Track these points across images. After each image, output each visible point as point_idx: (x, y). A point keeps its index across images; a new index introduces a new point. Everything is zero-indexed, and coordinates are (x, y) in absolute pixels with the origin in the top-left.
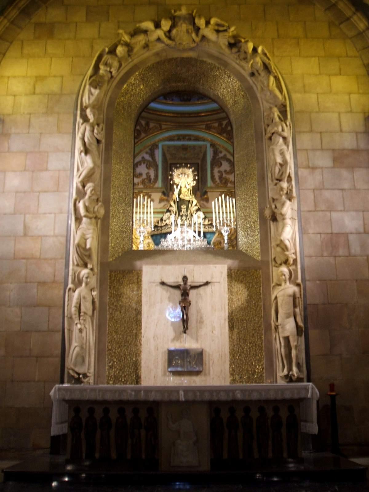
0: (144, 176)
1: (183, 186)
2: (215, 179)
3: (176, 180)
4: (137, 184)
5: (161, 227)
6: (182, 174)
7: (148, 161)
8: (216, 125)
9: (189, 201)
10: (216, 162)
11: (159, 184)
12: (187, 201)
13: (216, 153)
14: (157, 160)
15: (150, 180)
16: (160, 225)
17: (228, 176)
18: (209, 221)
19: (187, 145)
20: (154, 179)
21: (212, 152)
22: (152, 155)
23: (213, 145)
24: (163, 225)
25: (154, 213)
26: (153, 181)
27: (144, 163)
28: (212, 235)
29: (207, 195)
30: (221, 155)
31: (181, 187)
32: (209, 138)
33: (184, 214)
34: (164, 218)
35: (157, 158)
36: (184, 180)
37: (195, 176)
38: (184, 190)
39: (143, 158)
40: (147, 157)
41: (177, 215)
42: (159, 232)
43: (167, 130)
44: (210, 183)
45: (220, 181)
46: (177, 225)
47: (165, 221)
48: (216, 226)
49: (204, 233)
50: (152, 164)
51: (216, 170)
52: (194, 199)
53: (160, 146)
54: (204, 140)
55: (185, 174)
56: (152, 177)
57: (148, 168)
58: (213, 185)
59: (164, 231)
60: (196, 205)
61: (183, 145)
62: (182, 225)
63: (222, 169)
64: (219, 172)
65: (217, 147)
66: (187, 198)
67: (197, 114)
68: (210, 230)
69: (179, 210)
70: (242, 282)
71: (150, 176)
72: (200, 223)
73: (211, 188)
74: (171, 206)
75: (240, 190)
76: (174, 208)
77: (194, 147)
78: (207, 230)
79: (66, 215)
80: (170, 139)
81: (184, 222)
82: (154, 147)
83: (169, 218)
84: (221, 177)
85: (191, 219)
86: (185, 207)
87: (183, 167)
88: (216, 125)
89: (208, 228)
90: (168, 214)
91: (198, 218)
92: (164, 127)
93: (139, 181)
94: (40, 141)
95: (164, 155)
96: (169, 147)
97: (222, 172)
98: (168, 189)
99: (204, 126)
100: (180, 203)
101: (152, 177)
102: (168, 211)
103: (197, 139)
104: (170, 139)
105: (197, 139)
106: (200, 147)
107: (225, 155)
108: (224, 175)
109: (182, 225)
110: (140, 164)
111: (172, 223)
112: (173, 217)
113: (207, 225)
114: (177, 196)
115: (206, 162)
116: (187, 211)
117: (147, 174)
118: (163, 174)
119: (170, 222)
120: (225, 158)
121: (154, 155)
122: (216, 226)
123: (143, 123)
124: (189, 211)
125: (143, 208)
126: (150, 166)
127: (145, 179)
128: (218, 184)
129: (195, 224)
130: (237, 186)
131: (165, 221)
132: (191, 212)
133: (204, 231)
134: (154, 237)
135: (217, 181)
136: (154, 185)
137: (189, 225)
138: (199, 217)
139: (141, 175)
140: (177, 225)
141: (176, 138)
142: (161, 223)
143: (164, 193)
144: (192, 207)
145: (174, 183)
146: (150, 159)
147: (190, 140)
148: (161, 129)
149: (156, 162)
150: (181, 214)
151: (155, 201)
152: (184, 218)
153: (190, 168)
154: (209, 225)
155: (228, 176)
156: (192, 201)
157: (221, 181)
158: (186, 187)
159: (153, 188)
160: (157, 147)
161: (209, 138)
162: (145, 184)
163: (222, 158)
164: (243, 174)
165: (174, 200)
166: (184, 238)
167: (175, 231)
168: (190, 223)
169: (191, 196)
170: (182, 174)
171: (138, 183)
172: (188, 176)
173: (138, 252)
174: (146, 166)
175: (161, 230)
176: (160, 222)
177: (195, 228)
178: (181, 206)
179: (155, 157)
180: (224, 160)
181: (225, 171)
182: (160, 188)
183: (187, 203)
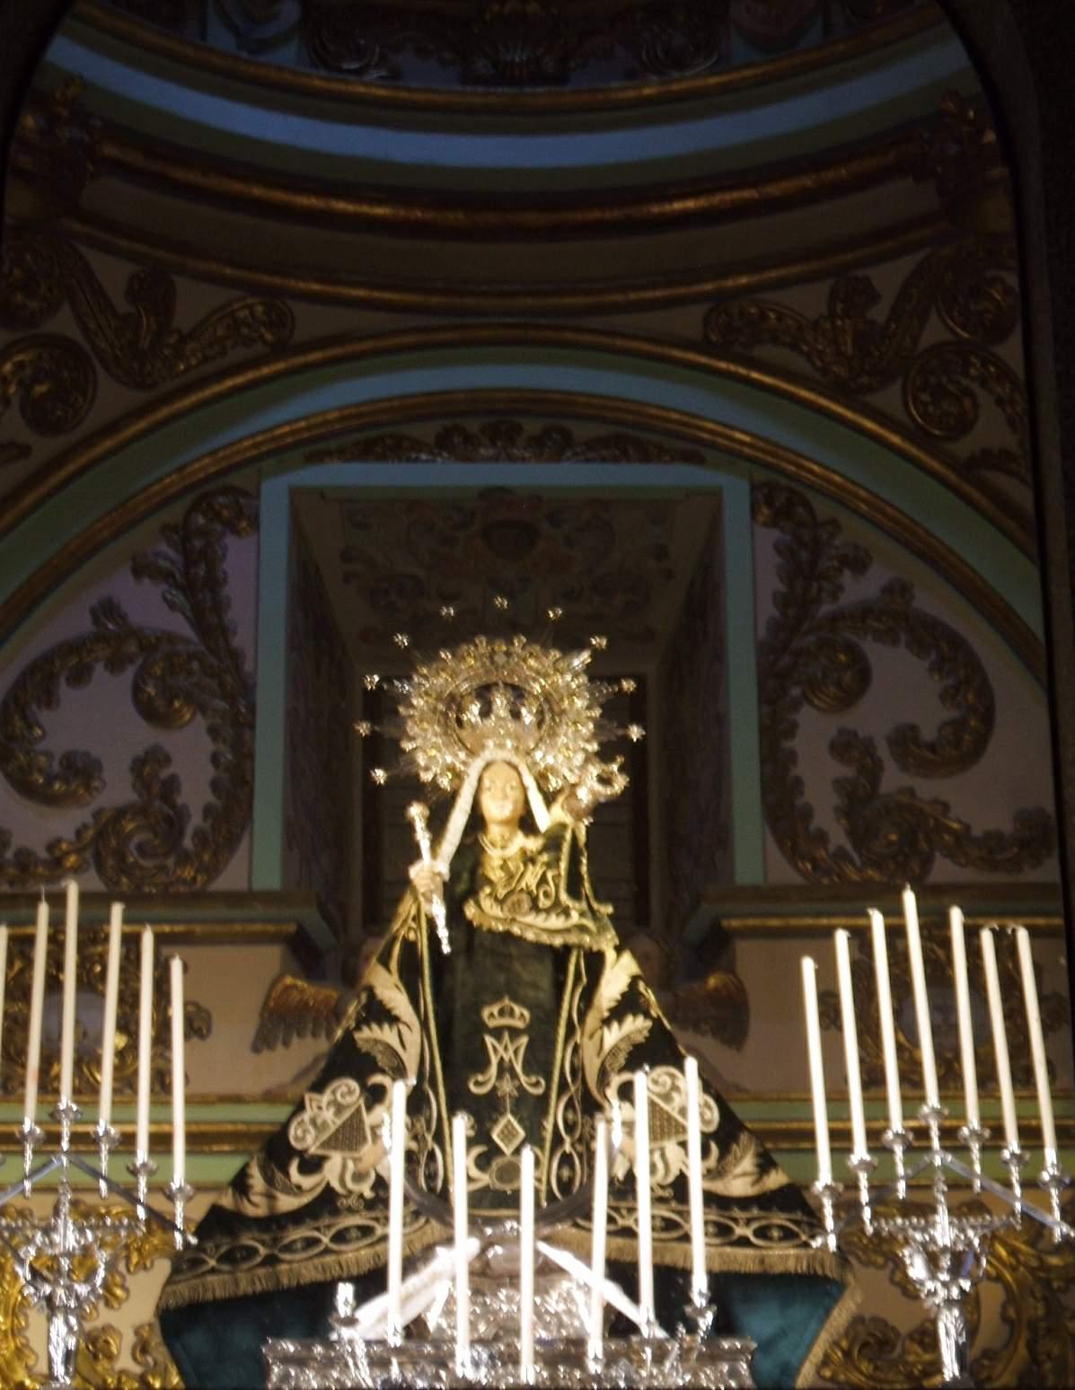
0: (117, 790)
1: (497, 809)
2: (807, 813)
3: (430, 754)
4: (43, 854)
5: (275, 1223)
6: (484, 693)
7: (150, 644)
8: (810, 301)
9: (559, 956)
10: (814, 656)
11: (261, 860)
12: (541, 949)
13: (807, 568)
14: (241, 640)
15: (173, 823)
16: (256, 1207)
17: (928, 789)
18: (765, 1164)
19: (535, 499)
20: (208, 811)
21: (770, 562)
22: (200, 588)
23: (781, 500)
24: (287, 1203)
25: (196, 1141)
26: (199, 835)
27: (115, 665)
28: (798, 1313)
29: (731, 970)
30: (858, 589)
31: (477, 821)
32: (744, 424)
33: (507, 1087)
34: (304, 1136)
35: (238, 613)
36: (512, 768)
37: (615, 711)
38: (504, 849)
39: (108, 609)
40: (152, 608)
41: (438, 1102)
42: (250, 1280)
43: (346, 354)
44: (753, 854)
45: (851, 833)
46: (431, 1202)
47: (312, 1165)
48: (847, 1207)
49: (721, 1283)
50: (189, 673)
51: (813, 730)
52: (607, 943)
53: (274, 497)
54: (689, 446)
55: (518, 693)
56: (196, 794)
57: (153, 713)
58: (785, 873)
59: (300, 1268)
60: (629, 1003)
61: (494, 495)
62: (494, 1202)
63: (874, 718)
64: (845, 746)
65: (824, 509)
66: (539, 927)
67: (617, 204)
68: (783, 1256)
69: (459, 1047)
71: (170, 788)
73: (767, 895)
74: (379, 1013)
76: (407, 1036)
77: (598, 511)
78: (744, 1260)
80: (374, 435)
81: (512, 1172)
82: (221, 504)
83: (351, 1135)
84: (858, 801)
85: (586, 1141)
86: (521, 1016)
87: (504, 628)
88: (810, 301)
89: (762, 1233)
90: (347, 1090)
91: (653, 1128)
92: (309, 321)
93: (68, 834)
95: (308, 593)
96: (357, 510)
98: (358, 821)
99: (689, 321)
100: (469, 974)
101: (196, 794)
102: (351, 1062)
103: (631, 436)
104: (374, 435)
105: (631, 436)
106: (658, 508)
107: (899, 590)
108: (893, 779)
109: (494, 1202)
110: (80, 676)
111: (381, 1184)
112: (392, 1126)
113: (744, 1203)
114: (439, 910)
115: (719, 656)
116: (539, 1060)
117: (148, 767)
118: (294, 772)
119: (359, 1177)
120: (895, 617)
121: (214, 582)
122: (847, 1207)
123: (114, 274)
124: (562, 1057)
125: (86, 1089)
126: (170, 694)
127: (120, 813)
128: (841, 855)
129: (623, 1189)
131: (312, 1165)
132: (578, 1071)
133: (716, 1268)
134: (197, 1340)
135: (822, 838)
136: (212, 871)
137: (564, 1207)
138: (665, 1126)
139: (81, 770)
140: (431, 1202)
141: (427, 431)
142: (269, 1180)
143: (303, 954)
144: (592, 1020)
145: (411, 787)
146: (180, 625)
147: (554, 445)
148: (280, 349)
149: (236, 656)
150: (479, 1085)
151: (218, 1026)
152: (507, 1128)
153: (569, 642)
154: (765, 1201)
155: (928, 789)
156: (595, 963)
157: (861, 835)
158: (526, 823)
159: (199, 897)
160: (244, 517)
161: (744, 424)
162: (121, 856)
163: (864, 615)
165: (410, 948)
166: (509, 1329)
167: (411, 1265)
168: (565, 1186)
169: (576, 908)
170: (484, 693)
171: (52, 846)
172: (550, 712)
174: (137, 690)
175: (271, 1261)
176: (257, 1181)
177: (630, 1233)
178: (476, 1009)
179: (219, 607)
180: (888, 637)
181: (905, 740)
182: (268, 897)
183: (542, 975)
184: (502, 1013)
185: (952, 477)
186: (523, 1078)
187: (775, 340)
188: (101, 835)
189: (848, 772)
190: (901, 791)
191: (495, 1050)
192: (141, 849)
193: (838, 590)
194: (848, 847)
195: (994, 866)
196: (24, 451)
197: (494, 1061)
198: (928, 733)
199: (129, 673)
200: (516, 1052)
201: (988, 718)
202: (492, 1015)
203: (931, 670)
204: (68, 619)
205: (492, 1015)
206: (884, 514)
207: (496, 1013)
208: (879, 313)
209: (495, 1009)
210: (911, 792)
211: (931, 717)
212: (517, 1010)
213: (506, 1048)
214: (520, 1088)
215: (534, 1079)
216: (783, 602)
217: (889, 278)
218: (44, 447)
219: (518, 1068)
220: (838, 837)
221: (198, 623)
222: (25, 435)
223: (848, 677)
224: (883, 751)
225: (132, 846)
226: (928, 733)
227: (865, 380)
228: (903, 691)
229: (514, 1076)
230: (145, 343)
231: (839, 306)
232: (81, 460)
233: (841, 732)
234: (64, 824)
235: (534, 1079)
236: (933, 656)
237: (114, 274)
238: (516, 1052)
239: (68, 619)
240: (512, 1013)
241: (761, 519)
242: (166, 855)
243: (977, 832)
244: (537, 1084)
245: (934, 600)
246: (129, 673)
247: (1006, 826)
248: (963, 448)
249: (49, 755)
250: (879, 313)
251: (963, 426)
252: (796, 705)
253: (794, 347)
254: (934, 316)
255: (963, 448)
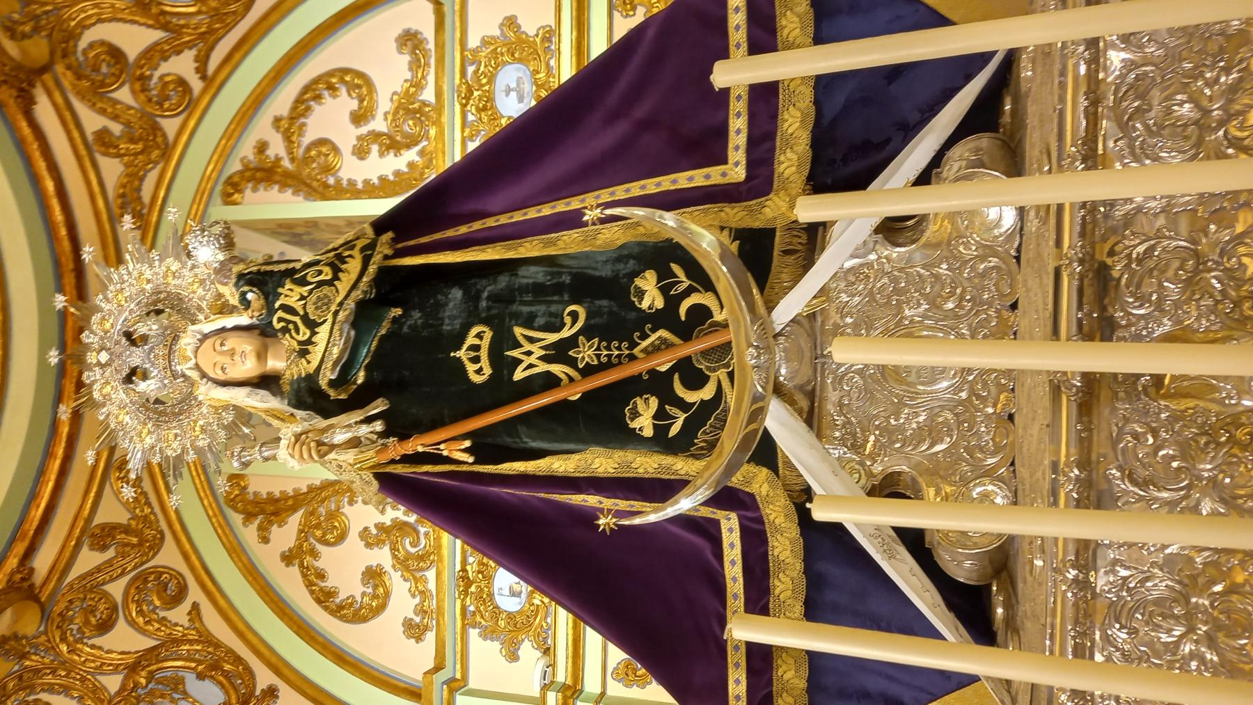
0: (382, 557)
2: (397, 173)
7: (304, 532)
13: (263, 173)
17: (384, 104)
30: (277, 147)
39: (288, 558)
40: (286, 534)
45: (408, 147)
63: (346, 136)
64: (361, 152)
108: (379, 124)
110: (321, 575)
117: (370, 540)
120: (290, 125)
121: (272, 500)
123: (88, 560)
127: (395, 557)
128: (422, 153)
139: (373, 575)
146: (295, 520)
149: (311, 489)
155: (384, 104)
157: (411, 142)
179: (285, 497)
181: (358, 118)
184: (476, 360)
185: (212, 91)
186: (566, 333)
187: (139, 190)
188: (407, 568)
189: (375, 148)
190: (386, 119)
191: (531, 366)
192: (414, 545)
193: (278, 159)
194: (417, 148)
195: (427, 64)
196: (195, 606)
197: (543, 367)
198: (354, 104)
199: (319, 547)
200: (531, 340)
201: (346, 71)
202: (479, 371)
203: (320, 104)
204: (290, 584)
205: (479, 371)
206: (234, 130)
207: (477, 366)
208: (116, 128)
209: (471, 368)
210: (386, 114)
211: (345, 103)
212: (471, 340)
213: (529, 353)
214: (588, 332)
215: (568, 320)
216: (284, 186)
217: (92, 121)
218: (195, 593)
219: (552, 338)
220: (411, 155)
221: (294, 509)
222: (186, 606)
223: (324, 150)
224: (364, 130)
225: (413, 550)
226: (354, 104)
227: (159, 140)
228: (332, 120)
229: (572, 342)
230: (135, 540)
231: (112, 151)
232: (202, 573)
233: (353, 153)
234: (399, 586)
235: (568, 320)
236: (312, 103)
237: (88, 560)
238: (531, 340)
239: (290, 584)
240: (476, 348)
241: (239, 200)
242: (417, 533)
243: (408, 76)
244: (575, 316)
245: (282, 101)
246: (319, 547)
247: (406, 58)
248: (196, 85)
249: (364, 594)
250: (116, 128)
251: (182, 82)
252: (338, 181)
253: (142, 179)
254: (113, 95)
255: (196, 85)
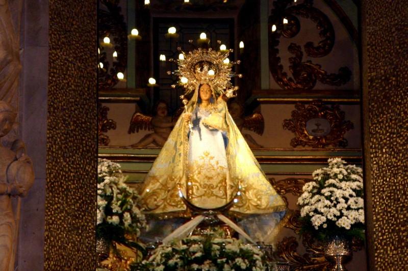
17: (315, 61)
29: (259, 112)
44: (267, 81)
45: (294, 74)
58: (275, 86)
70: (278, 248)
72: (214, 157)
73: (270, 92)
75: (379, 123)
79: (356, 207)
84: (296, 65)
94: (188, 137)
97: (299, 47)
130: (370, 111)
157: (296, 74)
164: (387, 79)
173: (114, 213)
181: (309, 45)
